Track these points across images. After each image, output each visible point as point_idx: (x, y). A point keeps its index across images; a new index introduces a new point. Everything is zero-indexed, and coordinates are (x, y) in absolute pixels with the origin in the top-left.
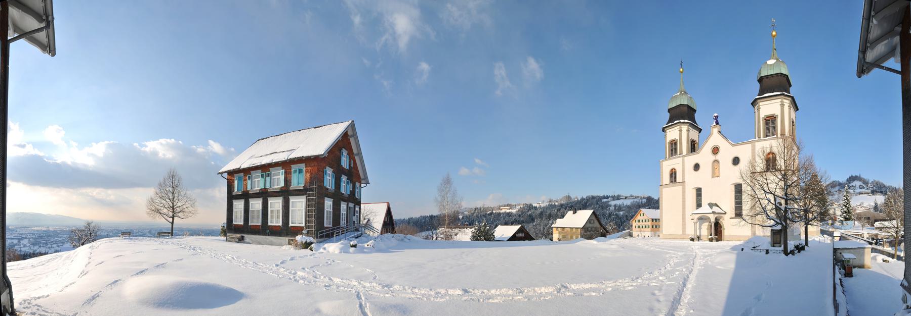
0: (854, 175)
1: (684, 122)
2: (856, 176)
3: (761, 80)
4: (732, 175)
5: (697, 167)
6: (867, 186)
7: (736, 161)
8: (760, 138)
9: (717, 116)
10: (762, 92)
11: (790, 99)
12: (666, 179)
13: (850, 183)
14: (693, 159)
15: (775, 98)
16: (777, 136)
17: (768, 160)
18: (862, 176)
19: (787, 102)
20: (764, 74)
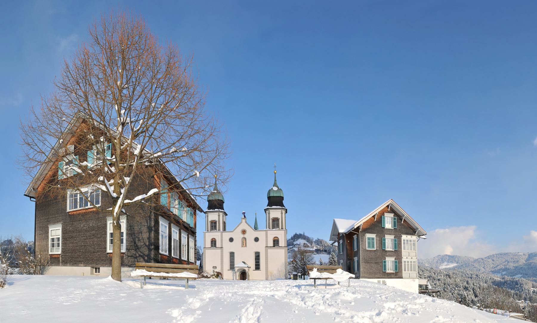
0: (298, 233)
1: (222, 211)
2: (301, 235)
3: (269, 198)
4: (253, 247)
5: (231, 240)
6: (311, 245)
7: (257, 240)
8: (270, 229)
9: (245, 213)
10: (270, 204)
11: (285, 210)
12: (208, 244)
13: (294, 241)
14: (227, 236)
15: (276, 209)
16: (279, 229)
17: (274, 241)
18: (306, 235)
19: (284, 212)
20: (272, 195)
